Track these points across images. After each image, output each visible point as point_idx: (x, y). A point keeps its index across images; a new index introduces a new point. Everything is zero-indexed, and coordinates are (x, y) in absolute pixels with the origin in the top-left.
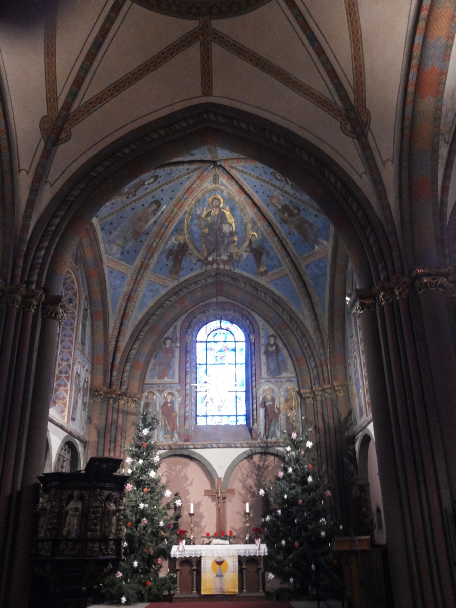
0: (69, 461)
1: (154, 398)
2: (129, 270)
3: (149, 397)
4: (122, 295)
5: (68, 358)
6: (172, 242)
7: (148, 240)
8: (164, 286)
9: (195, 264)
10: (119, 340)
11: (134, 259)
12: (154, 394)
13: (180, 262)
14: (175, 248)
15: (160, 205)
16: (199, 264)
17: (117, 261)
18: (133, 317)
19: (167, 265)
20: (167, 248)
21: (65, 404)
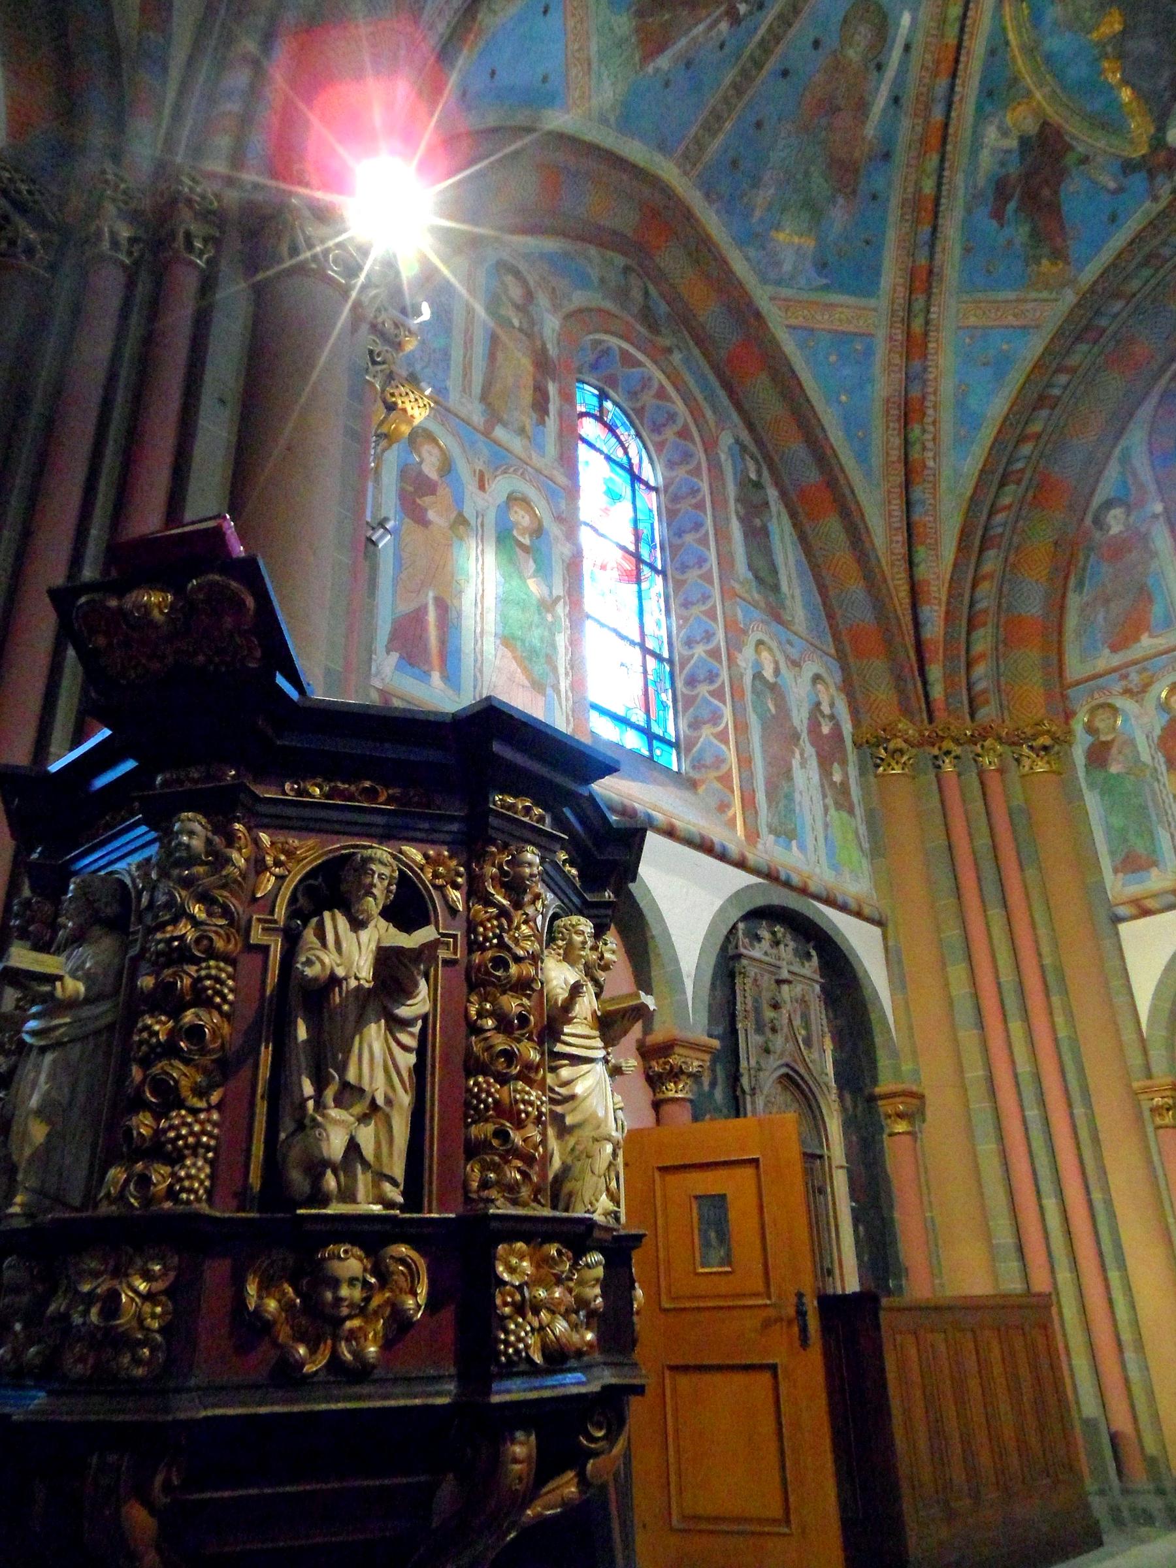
0: (817, 988)
1: (1119, 722)
2: (872, 315)
3: (1099, 724)
4: (878, 407)
5: (707, 632)
6: (994, 151)
7: (896, 184)
8: (1024, 327)
9: (1120, 190)
10: (916, 561)
11: (877, 272)
12: (1115, 710)
13: (1053, 209)
14: (1015, 157)
15: (885, 17)
16: (1138, 181)
17: (814, 296)
18: (946, 472)
19: (1010, 242)
20: (981, 182)
21: (726, 779)
